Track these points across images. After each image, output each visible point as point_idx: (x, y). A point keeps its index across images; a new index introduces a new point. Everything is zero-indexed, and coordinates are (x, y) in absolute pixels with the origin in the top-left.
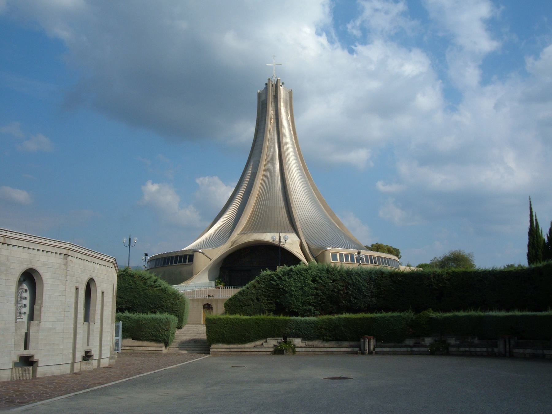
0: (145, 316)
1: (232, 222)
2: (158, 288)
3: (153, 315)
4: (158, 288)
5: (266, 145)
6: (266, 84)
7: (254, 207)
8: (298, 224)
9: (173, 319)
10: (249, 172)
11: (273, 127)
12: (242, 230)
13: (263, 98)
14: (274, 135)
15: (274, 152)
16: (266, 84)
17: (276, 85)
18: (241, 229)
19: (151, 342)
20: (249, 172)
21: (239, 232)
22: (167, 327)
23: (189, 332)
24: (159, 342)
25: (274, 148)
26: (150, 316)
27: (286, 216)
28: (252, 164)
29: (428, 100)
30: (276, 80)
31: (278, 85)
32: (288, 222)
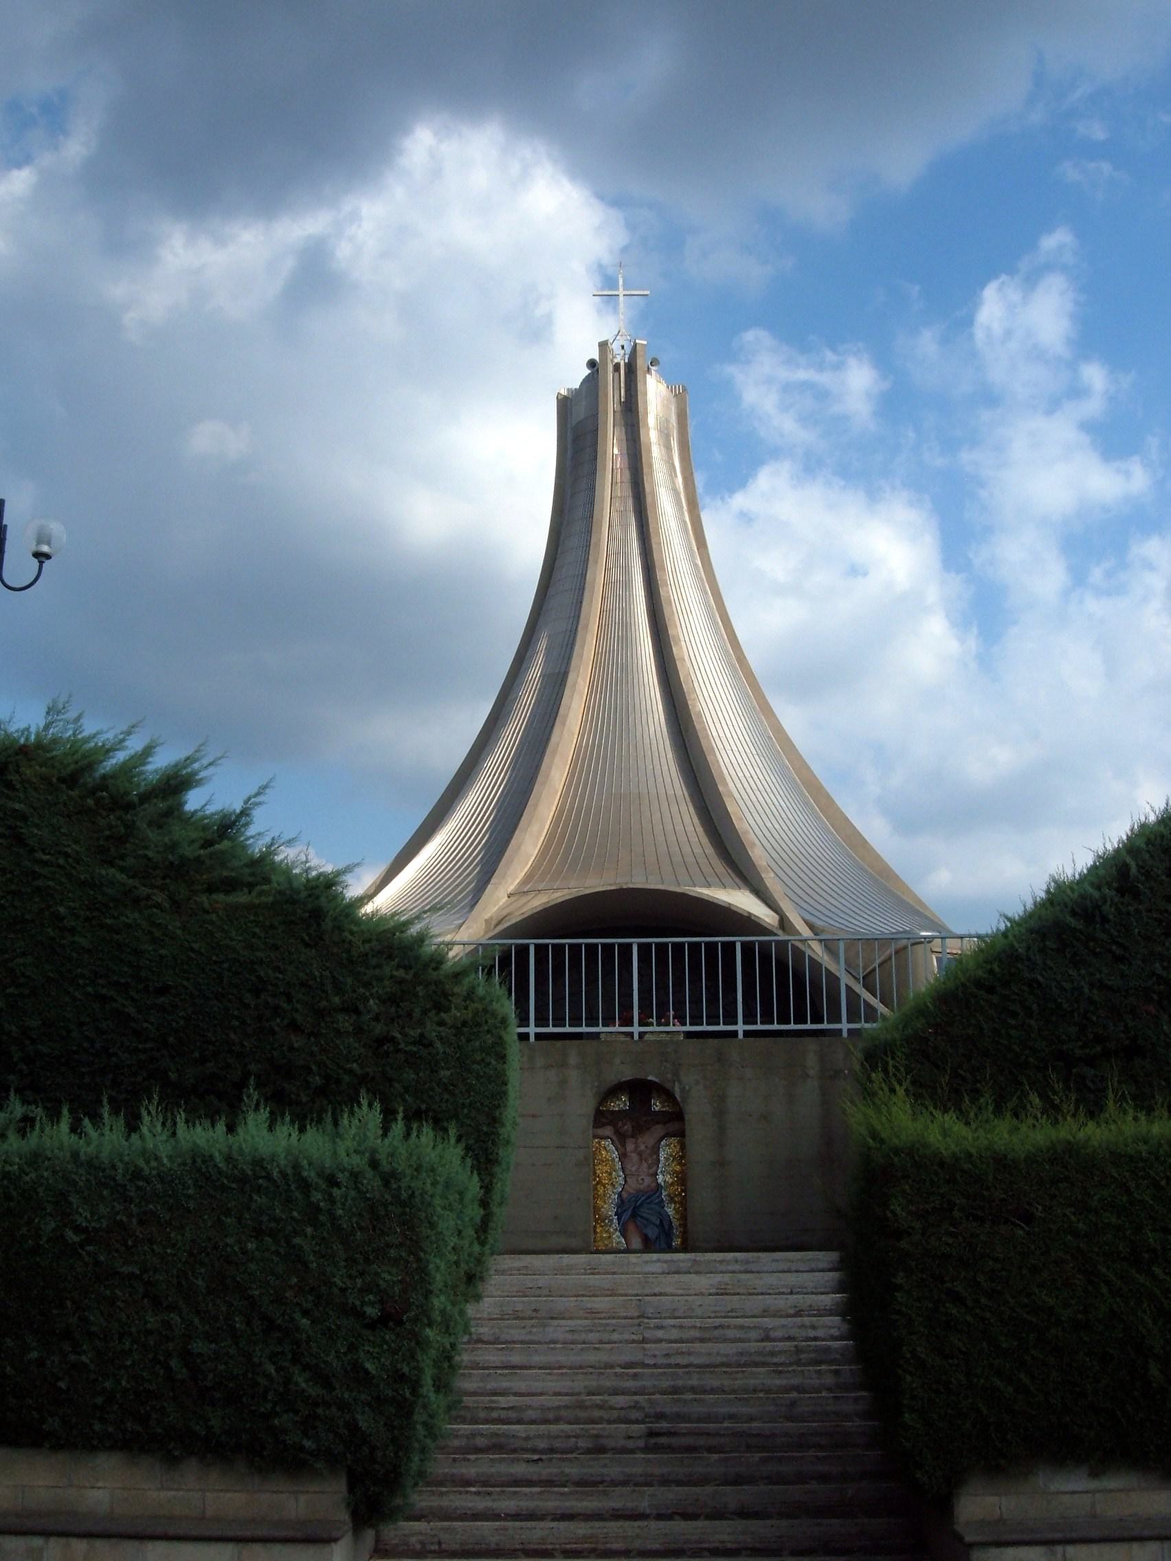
0: (106, 1139)
1: (478, 852)
2: (242, 898)
3: (206, 1137)
4: (242, 898)
5: (598, 577)
6: (592, 364)
7: (564, 797)
8: (759, 855)
9: (439, 1155)
10: (535, 672)
11: (622, 514)
12: (528, 878)
13: (580, 412)
14: (625, 541)
15: (628, 599)
16: (592, 364)
17: (631, 368)
18: (521, 875)
19: (172, 1461)
20: (535, 672)
21: (511, 888)
22: (388, 1276)
23: (557, 1330)
24: (286, 1462)
25: (628, 584)
26: (167, 1139)
27: (700, 830)
28: (542, 645)
29: (932, 645)
30: (628, 349)
31: (640, 362)
32: (710, 850)
